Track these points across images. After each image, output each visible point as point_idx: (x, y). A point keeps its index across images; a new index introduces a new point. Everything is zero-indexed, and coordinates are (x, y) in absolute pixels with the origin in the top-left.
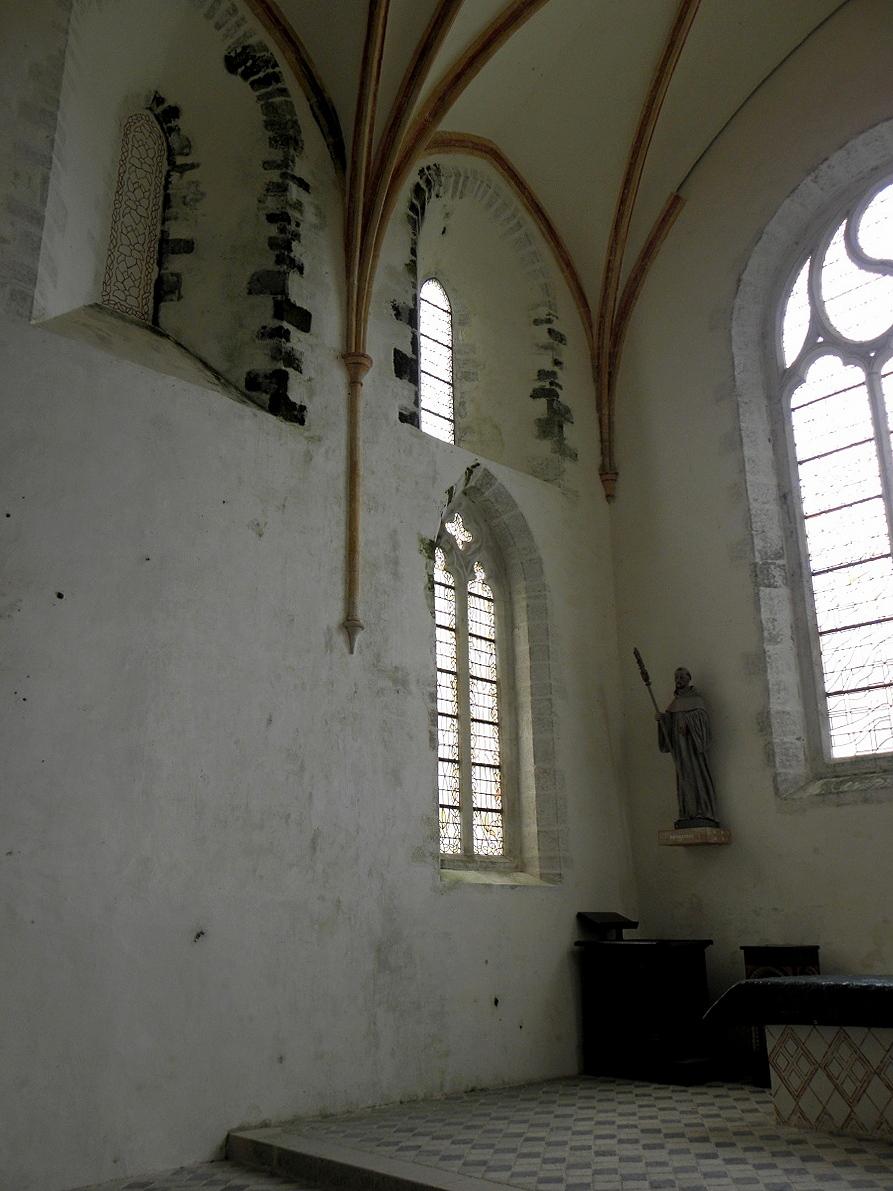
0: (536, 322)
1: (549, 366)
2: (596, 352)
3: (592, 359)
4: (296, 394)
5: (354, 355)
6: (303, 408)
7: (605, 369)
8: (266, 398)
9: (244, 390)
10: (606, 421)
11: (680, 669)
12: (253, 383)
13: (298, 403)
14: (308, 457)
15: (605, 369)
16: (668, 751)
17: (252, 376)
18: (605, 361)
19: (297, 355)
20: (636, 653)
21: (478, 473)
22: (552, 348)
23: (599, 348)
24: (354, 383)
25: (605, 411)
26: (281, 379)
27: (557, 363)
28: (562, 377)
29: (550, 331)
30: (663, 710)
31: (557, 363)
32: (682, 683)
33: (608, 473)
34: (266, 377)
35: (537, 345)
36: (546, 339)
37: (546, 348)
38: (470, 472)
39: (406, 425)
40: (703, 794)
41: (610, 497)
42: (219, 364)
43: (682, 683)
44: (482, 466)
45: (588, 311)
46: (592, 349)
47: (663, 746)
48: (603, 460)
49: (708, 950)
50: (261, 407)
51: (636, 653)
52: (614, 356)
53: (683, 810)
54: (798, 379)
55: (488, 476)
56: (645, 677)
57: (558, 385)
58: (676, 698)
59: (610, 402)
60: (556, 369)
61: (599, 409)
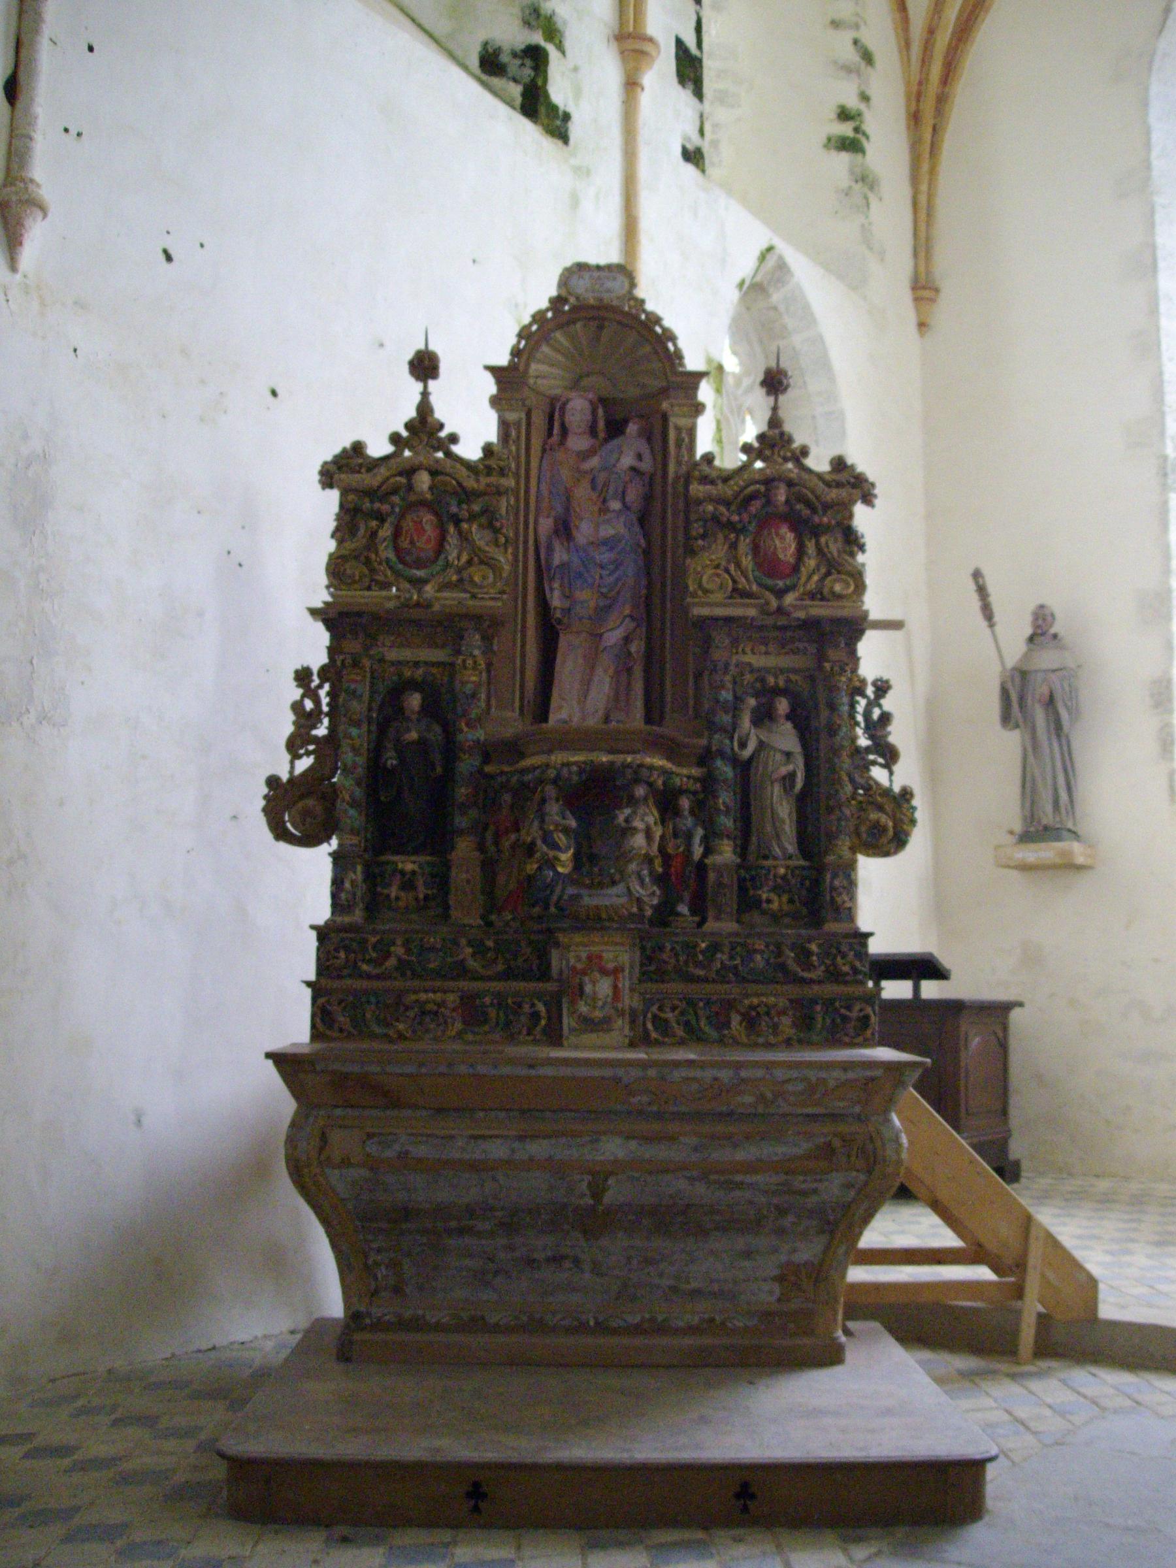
0: (835, 24)
1: (853, 103)
2: (915, 89)
3: (908, 100)
4: (559, 91)
5: (629, 36)
6: (567, 117)
7: (927, 116)
8: (516, 91)
9: (478, 71)
10: (923, 199)
11: (1042, 607)
12: (491, 64)
13: (562, 107)
14: (575, 201)
15: (927, 116)
16: (1017, 726)
17: (490, 50)
18: (928, 106)
19: (560, 25)
20: (977, 575)
21: (771, 262)
22: (858, 73)
23: (920, 83)
24: (631, 85)
25: (924, 187)
26: (535, 57)
27: (865, 98)
28: (870, 125)
29: (856, 42)
30: (1010, 663)
31: (865, 98)
32: (1042, 630)
33: (924, 289)
34: (515, 55)
35: (835, 62)
36: (850, 55)
37: (848, 69)
38: (763, 257)
39: (690, 169)
40: (1064, 796)
41: (922, 325)
42: (442, 27)
43: (1042, 630)
44: (777, 251)
45: (905, 20)
46: (908, 83)
47: (1006, 718)
48: (916, 266)
49: (1015, 1015)
50: (510, 103)
51: (977, 575)
52: (942, 100)
53: (1031, 815)
54: (581, 286)
55: (782, 266)
56: (988, 612)
57: (864, 134)
58: (1030, 650)
59: (933, 171)
60: (862, 106)
61: (915, 179)
